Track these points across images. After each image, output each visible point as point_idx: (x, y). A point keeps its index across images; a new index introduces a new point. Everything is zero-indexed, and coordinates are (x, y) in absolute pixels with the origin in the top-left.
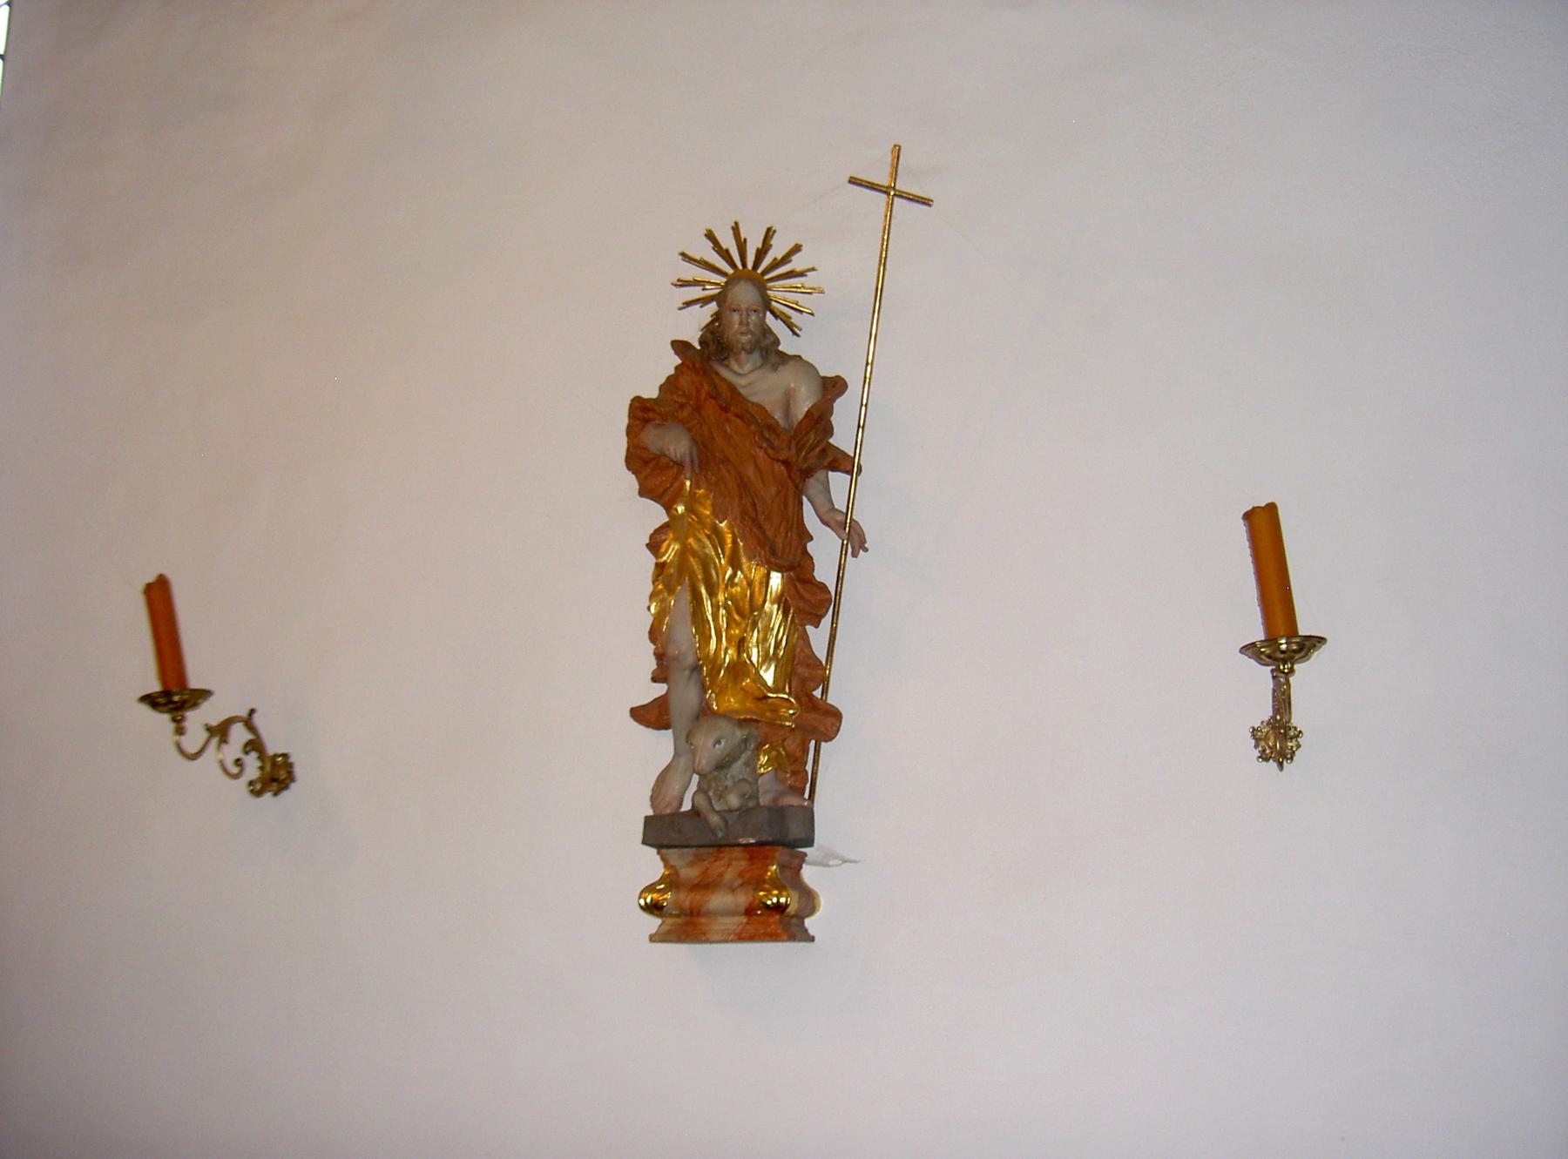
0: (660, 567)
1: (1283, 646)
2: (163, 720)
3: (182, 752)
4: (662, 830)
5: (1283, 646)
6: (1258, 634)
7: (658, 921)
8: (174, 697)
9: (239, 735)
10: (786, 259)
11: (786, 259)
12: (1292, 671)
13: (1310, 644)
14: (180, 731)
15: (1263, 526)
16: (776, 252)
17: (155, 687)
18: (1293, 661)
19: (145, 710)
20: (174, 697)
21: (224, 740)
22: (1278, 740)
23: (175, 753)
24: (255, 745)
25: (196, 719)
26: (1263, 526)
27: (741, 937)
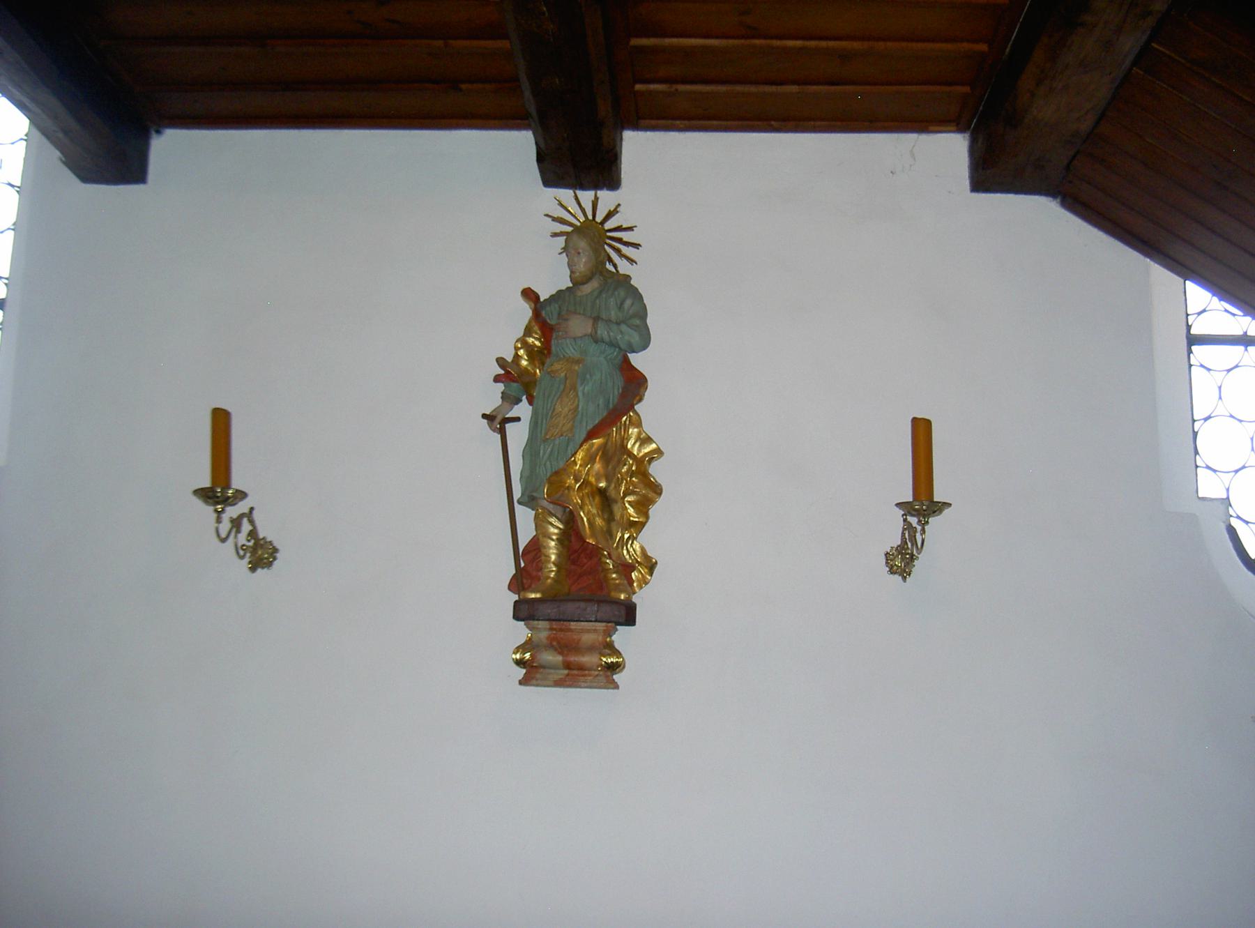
0: (639, 424)
1: (923, 505)
2: (208, 511)
3: (218, 535)
4: (628, 616)
5: (923, 505)
6: (908, 497)
7: (524, 671)
8: (218, 492)
9: (246, 527)
10: (627, 244)
11: (627, 244)
12: (223, 510)
13: (937, 508)
14: (219, 520)
15: (922, 431)
16: (625, 236)
17: (206, 483)
18: (929, 516)
19: (199, 504)
20: (218, 492)
21: (238, 531)
22: (902, 560)
23: (214, 535)
24: (253, 534)
25: (232, 512)
26: (922, 431)
27: (559, 683)
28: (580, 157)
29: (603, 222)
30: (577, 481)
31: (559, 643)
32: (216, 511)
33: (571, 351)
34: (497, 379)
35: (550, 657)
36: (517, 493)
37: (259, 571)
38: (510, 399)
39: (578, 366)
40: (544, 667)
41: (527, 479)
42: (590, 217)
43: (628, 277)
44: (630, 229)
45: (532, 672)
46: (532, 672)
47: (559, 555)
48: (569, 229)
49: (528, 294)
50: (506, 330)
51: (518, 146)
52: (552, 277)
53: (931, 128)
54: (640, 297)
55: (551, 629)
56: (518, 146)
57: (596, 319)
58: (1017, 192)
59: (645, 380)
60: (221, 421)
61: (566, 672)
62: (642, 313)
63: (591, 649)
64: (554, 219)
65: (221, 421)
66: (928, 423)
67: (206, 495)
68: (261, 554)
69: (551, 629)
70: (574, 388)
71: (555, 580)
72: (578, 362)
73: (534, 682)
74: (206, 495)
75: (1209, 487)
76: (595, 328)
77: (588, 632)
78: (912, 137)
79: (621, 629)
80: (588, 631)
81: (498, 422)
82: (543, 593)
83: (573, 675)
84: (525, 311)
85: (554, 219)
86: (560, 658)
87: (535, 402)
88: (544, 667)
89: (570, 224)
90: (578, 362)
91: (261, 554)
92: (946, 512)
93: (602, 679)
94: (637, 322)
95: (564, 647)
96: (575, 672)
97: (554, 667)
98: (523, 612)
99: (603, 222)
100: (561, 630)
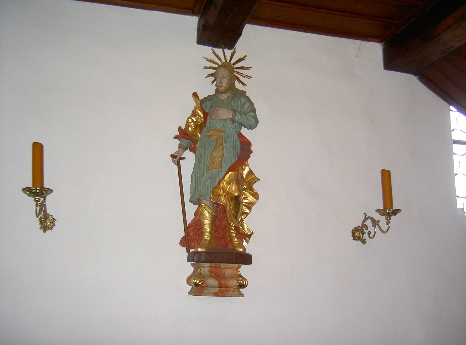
5: (38, 190)
15: (386, 176)
19: (25, 196)
26: (386, 176)
27: (216, 295)
28: (220, 32)
29: (234, 64)
30: (224, 192)
31: (215, 274)
32: (35, 200)
33: (219, 126)
34: (176, 137)
35: (211, 282)
36: (187, 196)
37: (47, 231)
38: (182, 148)
39: (217, 136)
40: (208, 287)
41: (194, 189)
42: (228, 60)
43: (245, 92)
44: (248, 68)
45: (198, 289)
46: (198, 289)
47: (211, 229)
48: (217, 66)
49: (195, 95)
50: (181, 113)
51: (190, 23)
52: (207, 89)
53: (369, 39)
54: (252, 103)
55: (211, 267)
56: (190, 23)
57: (234, 111)
58: (402, 71)
59: (251, 144)
60: (38, 149)
61: (219, 289)
62: (254, 110)
63: (232, 277)
64: (207, 60)
65: (38, 149)
66: (389, 172)
67: (28, 191)
68: (46, 222)
69: (211, 267)
70: (222, 144)
71: (210, 241)
72: (223, 131)
73: (203, 294)
74: (28, 191)
75: (459, 206)
76: (234, 116)
77: (228, 269)
78: (360, 42)
79: (244, 266)
80: (229, 268)
81: (177, 159)
82: (206, 248)
83: (223, 290)
84: (193, 104)
85: (207, 60)
86: (217, 282)
87: (198, 151)
88: (208, 287)
89: (216, 63)
90: (223, 131)
91: (46, 222)
92: (399, 214)
93: (236, 292)
94: (252, 114)
95: (219, 276)
96: (223, 289)
97: (213, 287)
98: (193, 258)
99: (234, 64)
100: (215, 267)
